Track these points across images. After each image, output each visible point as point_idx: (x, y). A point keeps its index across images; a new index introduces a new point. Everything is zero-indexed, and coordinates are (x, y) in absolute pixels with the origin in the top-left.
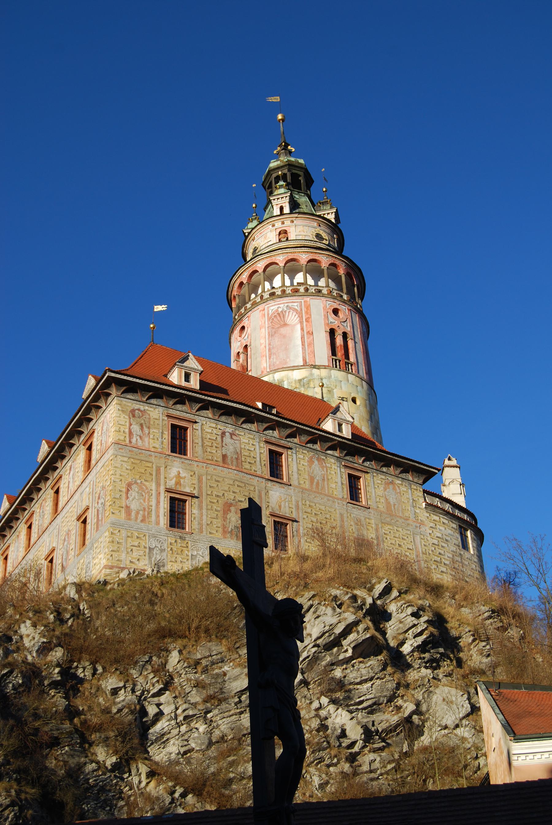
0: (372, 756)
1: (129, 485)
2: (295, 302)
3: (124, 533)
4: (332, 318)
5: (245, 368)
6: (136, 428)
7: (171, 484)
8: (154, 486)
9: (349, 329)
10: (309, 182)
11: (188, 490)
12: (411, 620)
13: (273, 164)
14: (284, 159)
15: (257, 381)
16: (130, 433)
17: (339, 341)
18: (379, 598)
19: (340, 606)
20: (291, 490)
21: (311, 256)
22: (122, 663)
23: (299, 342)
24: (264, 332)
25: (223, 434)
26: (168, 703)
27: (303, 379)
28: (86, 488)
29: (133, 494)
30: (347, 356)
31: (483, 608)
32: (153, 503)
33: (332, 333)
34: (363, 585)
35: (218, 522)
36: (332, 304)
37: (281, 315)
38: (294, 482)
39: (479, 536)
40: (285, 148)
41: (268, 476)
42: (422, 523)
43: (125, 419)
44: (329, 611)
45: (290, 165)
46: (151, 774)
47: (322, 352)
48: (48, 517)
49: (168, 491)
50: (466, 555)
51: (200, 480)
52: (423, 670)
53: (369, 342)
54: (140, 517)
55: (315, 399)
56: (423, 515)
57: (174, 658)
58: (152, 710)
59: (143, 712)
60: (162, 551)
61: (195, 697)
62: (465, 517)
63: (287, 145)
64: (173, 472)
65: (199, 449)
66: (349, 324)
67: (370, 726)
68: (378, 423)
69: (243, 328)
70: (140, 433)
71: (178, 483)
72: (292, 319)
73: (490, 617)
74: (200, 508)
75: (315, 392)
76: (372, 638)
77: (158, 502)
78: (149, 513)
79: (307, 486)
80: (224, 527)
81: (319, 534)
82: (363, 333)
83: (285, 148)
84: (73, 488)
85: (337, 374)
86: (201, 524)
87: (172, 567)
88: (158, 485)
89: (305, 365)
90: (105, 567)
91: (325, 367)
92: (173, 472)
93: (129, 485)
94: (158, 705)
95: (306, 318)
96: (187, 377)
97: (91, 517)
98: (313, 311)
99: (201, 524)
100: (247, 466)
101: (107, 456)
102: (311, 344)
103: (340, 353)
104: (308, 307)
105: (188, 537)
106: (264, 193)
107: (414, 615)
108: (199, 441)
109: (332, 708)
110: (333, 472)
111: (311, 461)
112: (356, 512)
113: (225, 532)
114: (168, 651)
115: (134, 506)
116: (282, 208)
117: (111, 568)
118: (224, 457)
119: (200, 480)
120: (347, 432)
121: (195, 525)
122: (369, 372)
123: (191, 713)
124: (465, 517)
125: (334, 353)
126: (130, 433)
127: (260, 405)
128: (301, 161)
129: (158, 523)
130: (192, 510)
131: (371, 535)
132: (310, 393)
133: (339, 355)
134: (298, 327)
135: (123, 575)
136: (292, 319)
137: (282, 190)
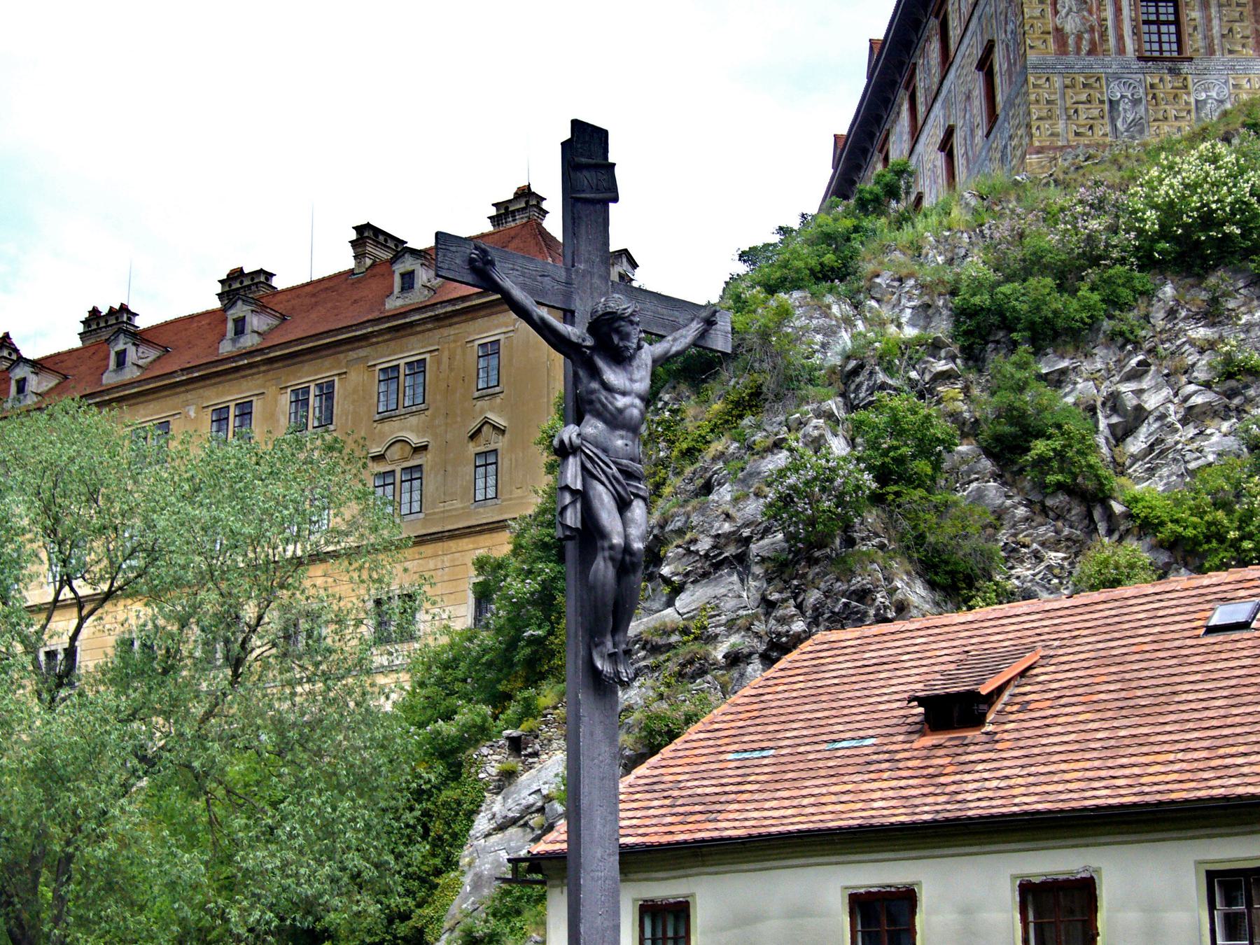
3: (1057, 82)
26: (1157, 388)
32: (1109, 14)
48: (936, 70)
54: (1085, 46)
60: (1136, 102)
78: (1103, 35)
86: (1208, 38)
99: (1208, 38)
129: (1121, 50)
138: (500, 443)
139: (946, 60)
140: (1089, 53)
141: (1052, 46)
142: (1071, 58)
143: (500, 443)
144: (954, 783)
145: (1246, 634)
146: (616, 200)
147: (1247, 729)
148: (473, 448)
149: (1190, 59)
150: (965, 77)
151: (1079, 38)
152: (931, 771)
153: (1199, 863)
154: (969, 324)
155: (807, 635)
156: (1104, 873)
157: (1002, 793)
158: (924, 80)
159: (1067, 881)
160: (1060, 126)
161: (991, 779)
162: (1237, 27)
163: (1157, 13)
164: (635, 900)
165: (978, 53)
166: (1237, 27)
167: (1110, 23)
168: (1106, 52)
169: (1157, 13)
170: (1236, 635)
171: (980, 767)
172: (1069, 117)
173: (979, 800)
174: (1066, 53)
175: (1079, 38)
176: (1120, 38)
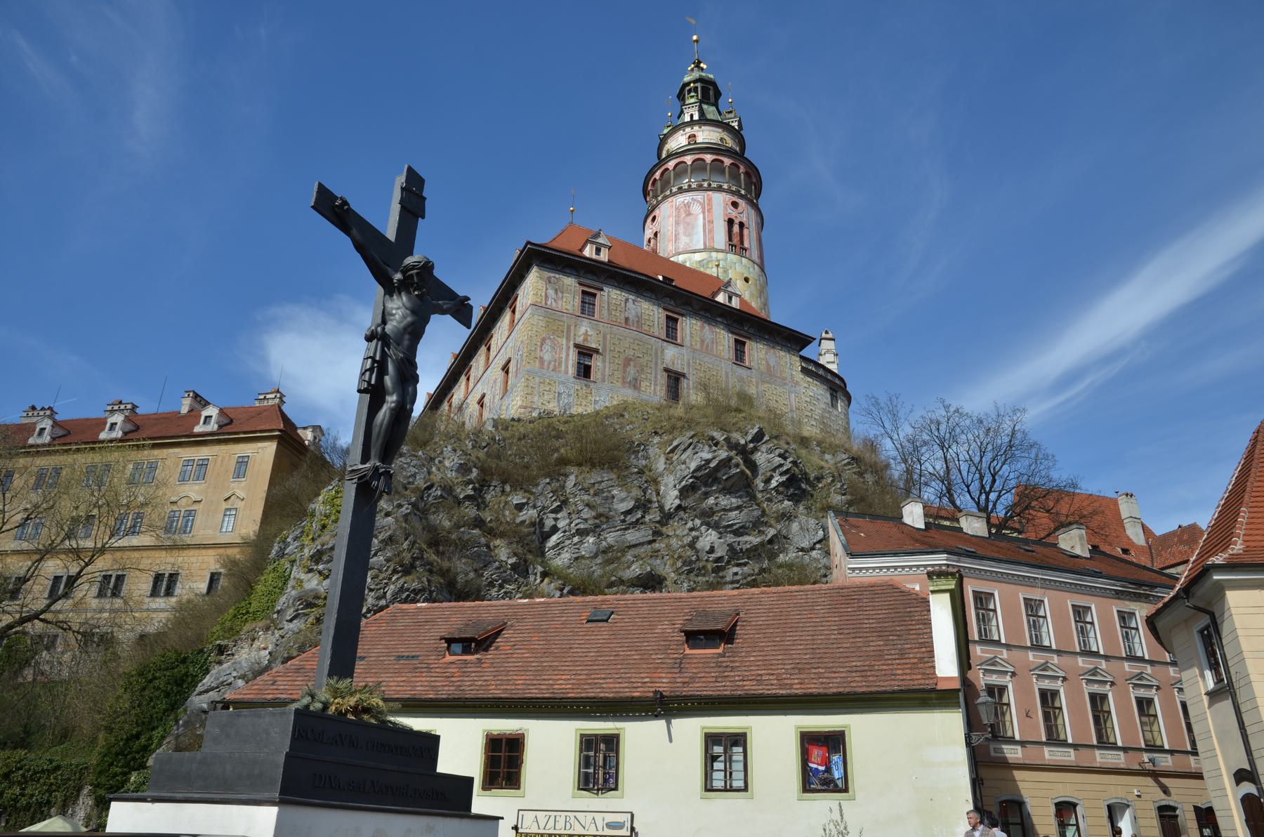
0: (735, 569)
1: (543, 340)
2: (699, 196)
3: (537, 379)
4: (730, 210)
5: (655, 251)
6: (551, 292)
7: (580, 340)
8: (564, 341)
9: (744, 220)
10: (718, 94)
11: (594, 346)
12: (778, 460)
13: (687, 79)
14: (696, 74)
15: (667, 260)
16: (546, 296)
17: (736, 228)
18: (751, 441)
19: (716, 445)
20: (684, 350)
21: (715, 157)
22: (522, 482)
23: (701, 229)
24: (672, 220)
25: (627, 300)
26: (564, 518)
27: (1225, 690)
28: (510, 343)
29: (547, 347)
30: (742, 242)
31: (844, 456)
32: (564, 355)
33: (730, 222)
34: (739, 430)
35: (618, 374)
36: (730, 198)
37: (687, 205)
38: (687, 343)
39: (848, 398)
40: (698, 66)
41: (664, 337)
42: (797, 383)
43: (542, 284)
44: (707, 448)
45: (700, 80)
46: (544, 575)
47: (721, 239)
48: (481, 369)
49: (576, 346)
50: (835, 412)
51: (605, 338)
52: (786, 502)
53: (764, 233)
54: (551, 367)
55: (711, 276)
56: (799, 376)
57: (571, 480)
58: (549, 523)
59: (541, 523)
60: (569, 395)
61: (587, 514)
62: (837, 381)
63: (700, 62)
64: (582, 330)
65: (605, 312)
66: (745, 215)
67: (735, 545)
68: (766, 300)
69: (654, 218)
70: (554, 296)
71: (585, 340)
72: (696, 209)
73: (849, 463)
74: (604, 361)
75: (713, 271)
76: (742, 472)
77: (568, 355)
78: (560, 364)
79: (698, 347)
80: (624, 378)
81: (704, 387)
82: (757, 224)
83: (698, 66)
84: (500, 344)
85: (732, 257)
86: (603, 375)
87: (576, 410)
88: (568, 340)
89: (705, 250)
90: (521, 407)
91: (722, 251)
92: (582, 330)
93: (543, 340)
94: (556, 519)
95: (707, 208)
96: (598, 251)
97: (512, 367)
98: (715, 202)
99: (603, 375)
100: (646, 328)
101: (527, 315)
102: (711, 231)
103: (736, 240)
104: (710, 200)
105: (592, 385)
106: (678, 103)
107: (780, 456)
108: (606, 305)
109: (703, 528)
110: (724, 340)
111: (702, 327)
112: (740, 371)
113: (624, 382)
114: (566, 476)
115: (547, 357)
116: (692, 116)
117: (525, 408)
118: (627, 319)
119: (605, 338)
120: (735, 303)
121: (599, 376)
122: (761, 256)
123: (582, 526)
124: (837, 381)
125: (730, 239)
126: (546, 296)
127: (660, 278)
128: (711, 76)
129: (567, 372)
130: (596, 363)
131: (752, 391)
132: (708, 272)
133: (736, 244)
134: (701, 216)
135: (535, 414)
136: (696, 209)
137: (693, 100)
138: (239, 504)
139: (513, 323)
141: (537, 364)
143: (239, 504)
145: (605, 624)
146: (423, 217)
148: (225, 505)
150: (495, 372)
155: (387, 606)
158: (474, 373)
160: (536, 398)
161: (481, 676)
165: (479, 396)
170: (600, 624)
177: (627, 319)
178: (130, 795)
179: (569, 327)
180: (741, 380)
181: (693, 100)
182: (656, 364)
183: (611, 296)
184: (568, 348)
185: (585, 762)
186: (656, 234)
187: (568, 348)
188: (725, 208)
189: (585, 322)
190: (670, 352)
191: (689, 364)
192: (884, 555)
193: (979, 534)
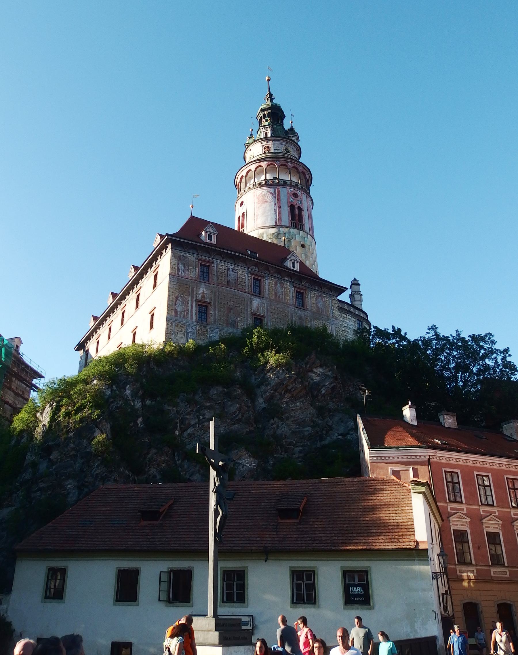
1: (177, 298)
6: (181, 266)
11: (208, 300)
29: (179, 302)
32: (190, 308)
42: (336, 318)
51: (215, 294)
69: (242, 203)
71: (203, 296)
74: (215, 311)
77: (192, 307)
92: (201, 290)
100: (240, 287)
113: (227, 324)
115: (179, 309)
118: (228, 282)
119: (215, 294)
120: (297, 268)
129: (191, 318)
137: (267, 123)
140: (183, 317)
142: (178, 318)
144: (152, 538)
147: (234, 530)
149: (209, 324)
151: (181, 313)
152: (144, 534)
153: (291, 567)
154: (410, 505)
156: (249, 569)
157: (167, 543)
159: (183, 570)
162: (222, 318)
163: (202, 310)
164: (47, 567)
166: (222, 318)
167: (189, 310)
168: (187, 318)
169: (202, 310)
171: (159, 534)
172: (175, 334)
173: (160, 544)
174: (177, 316)
175: (181, 313)
176: (192, 315)
177: (228, 282)
178: (295, 592)
179: (192, 290)
180: (301, 318)
181: (267, 123)
182: (247, 310)
183: (219, 265)
184: (192, 303)
185: (366, 587)
186: (243, 214)
187: (192, 303)
188: (288, 198)
189: (203, 285)
190: (256, 302)
191: (268, 310)
192: (392, 550)
193: (451, 427)
